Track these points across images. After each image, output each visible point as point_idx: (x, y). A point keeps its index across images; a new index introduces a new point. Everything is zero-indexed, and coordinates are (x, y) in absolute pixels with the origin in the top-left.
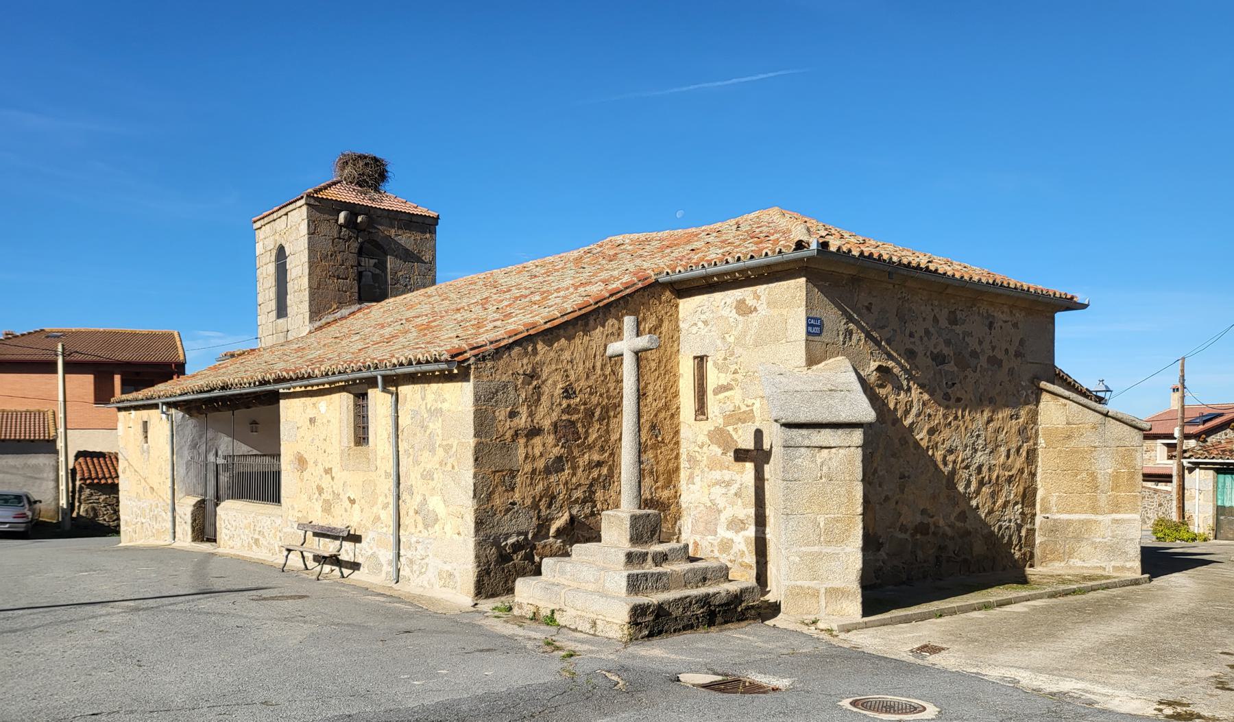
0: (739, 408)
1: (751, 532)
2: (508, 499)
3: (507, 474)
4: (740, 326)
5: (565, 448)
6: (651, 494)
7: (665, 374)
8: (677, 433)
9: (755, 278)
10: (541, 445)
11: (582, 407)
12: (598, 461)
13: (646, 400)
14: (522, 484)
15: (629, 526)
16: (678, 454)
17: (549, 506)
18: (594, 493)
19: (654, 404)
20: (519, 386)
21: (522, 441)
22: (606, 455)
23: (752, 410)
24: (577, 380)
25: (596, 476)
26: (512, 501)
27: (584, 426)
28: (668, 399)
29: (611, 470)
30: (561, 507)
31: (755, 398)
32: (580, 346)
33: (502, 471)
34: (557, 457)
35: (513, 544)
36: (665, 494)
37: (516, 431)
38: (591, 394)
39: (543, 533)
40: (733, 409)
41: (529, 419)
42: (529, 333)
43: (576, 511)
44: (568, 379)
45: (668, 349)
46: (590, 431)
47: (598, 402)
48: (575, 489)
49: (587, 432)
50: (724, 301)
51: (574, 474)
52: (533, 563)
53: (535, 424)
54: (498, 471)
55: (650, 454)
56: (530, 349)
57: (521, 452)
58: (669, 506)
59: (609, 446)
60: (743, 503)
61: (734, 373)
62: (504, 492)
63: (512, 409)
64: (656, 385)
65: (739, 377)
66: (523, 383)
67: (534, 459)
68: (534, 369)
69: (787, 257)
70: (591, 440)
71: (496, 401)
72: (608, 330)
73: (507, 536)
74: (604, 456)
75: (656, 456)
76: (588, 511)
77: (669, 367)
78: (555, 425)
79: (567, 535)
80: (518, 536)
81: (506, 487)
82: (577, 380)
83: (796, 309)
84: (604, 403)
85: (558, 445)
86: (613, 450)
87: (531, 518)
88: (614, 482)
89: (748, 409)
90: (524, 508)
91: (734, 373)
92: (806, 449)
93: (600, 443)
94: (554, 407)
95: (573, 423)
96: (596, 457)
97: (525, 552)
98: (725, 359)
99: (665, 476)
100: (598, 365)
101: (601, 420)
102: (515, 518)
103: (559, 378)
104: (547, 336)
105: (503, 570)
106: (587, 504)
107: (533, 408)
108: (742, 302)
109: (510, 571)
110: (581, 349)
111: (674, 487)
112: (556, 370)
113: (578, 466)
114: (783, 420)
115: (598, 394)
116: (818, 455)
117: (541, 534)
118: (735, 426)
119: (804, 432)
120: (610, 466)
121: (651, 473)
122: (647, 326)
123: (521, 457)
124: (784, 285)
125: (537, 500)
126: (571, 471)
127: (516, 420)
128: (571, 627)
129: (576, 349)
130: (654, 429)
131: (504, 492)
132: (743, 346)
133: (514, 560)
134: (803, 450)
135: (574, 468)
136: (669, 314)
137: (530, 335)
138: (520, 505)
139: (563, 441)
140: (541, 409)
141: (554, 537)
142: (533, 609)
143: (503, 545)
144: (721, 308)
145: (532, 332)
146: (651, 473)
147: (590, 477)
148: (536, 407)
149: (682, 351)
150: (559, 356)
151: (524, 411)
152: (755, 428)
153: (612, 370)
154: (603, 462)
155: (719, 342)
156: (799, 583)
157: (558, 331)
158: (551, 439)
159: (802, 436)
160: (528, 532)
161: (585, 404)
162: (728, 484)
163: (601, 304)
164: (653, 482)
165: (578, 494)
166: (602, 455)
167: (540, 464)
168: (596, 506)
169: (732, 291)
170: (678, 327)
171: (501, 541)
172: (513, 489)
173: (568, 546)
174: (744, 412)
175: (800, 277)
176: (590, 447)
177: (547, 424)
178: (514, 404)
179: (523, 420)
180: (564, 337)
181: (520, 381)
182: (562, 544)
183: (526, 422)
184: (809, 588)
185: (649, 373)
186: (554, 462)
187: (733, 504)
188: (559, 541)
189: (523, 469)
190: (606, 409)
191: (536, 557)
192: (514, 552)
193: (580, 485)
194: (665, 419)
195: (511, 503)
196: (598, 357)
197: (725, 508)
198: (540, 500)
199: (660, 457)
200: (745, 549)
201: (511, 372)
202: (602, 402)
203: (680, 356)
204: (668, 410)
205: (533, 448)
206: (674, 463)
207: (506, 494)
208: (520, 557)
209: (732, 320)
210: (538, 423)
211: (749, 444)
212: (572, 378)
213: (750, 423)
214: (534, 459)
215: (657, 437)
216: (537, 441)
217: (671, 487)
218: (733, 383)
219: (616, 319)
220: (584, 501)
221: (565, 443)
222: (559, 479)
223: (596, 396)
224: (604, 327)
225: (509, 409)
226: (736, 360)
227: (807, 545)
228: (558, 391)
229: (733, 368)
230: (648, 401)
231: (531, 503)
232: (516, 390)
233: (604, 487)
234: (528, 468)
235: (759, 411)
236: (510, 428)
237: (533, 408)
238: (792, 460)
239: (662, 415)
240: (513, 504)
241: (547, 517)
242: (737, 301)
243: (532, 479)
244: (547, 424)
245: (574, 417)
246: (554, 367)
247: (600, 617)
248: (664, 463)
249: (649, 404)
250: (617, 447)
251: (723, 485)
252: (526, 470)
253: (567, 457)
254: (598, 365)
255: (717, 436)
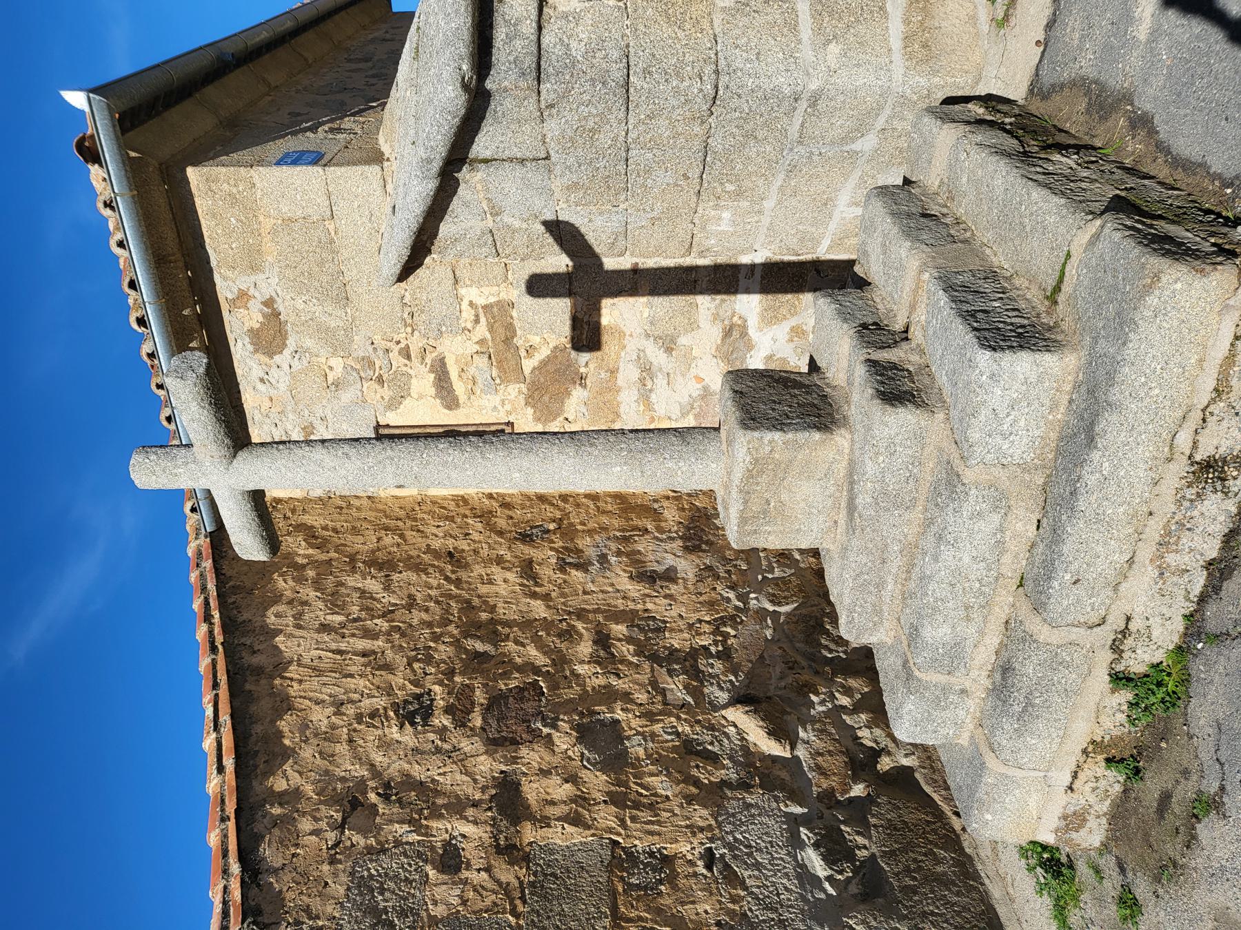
0: (482, 342)
1: (749, 305)
2: (695, 875)
3: (622, 878)
4: (308, 343)
5: (557, 719)
6: (673, 539)
7: (415, 520)
8: (542, 498)
9: (201, 301)
10: (545, 782)
11: (458, 679)
12: (595, 642)
13: (463, 551)
14: (652, 833)
15: (777, 436)
16: (587, 496)
17: (713, 759)
18: (673, 651)
19: (476, 536)
20: (372, 841)
21: (529, 834)
22: (580, 626)
23: (485, 307)
24: (389, 691)
25: (631, 648)
26: (700, 863)
27: (506, 675)
28: (468, 513)
29: (618, 616)
30: (712, 728)
31: (459, 299)
32: (306, 686)
33: (614, 894)
34: (577, 738)
35: (829, 860)
36: (671, 515)
37: (499, 850)
38: (429, 660)
39: (784, 775)
40: (486, 359)
41: (470, 812)
42: (232, 816)
43: (718, 693)
44: (382, 711)
45: (363, 515)
46: (518, 660)
47: (451, 644)
48: (665, 696)
49: (519, 669)
50: (260, 386)
51: (626, 697)
52: (869, 800)
53: (486, 797)
54: (614, 908)
55: (584, 542)
56: (276, 811)
57: (562, 836)
58: (698, 509)
59: (561, 621)
60: (686, 331)
61: (409, 357)
62: (675, 887)
63: (433, 863)
64: (433, 534)
65: (416, 343)
66: (364, 832)
67: (582, 800)
68: (334, 800)
69: (120, 182)
70: (541, 660)
71: (403, 914)
72: (287, 626)
73: (805, 877)
74: (583, 631)
75: (590, 532)
76: (718, 666)
77: (402, 513)
78: (494, 744)
79: (784, 712)
80: (801, 845)
81: (661, 882)
82: (389, 691)
83: (259, 194)
84: (455, 632)
85: (549, 735)
86: (569, 613)
87: (748, 806)
88: (646, 610)
89: (483, 319)
90: (719, 825)
91: (409, 357)
92: (544, 31)
93: (553, 641)
94: (446, 746)
95: (496, 702)
96: (585, 648)
97: (845, 823)
98: (380, 380)
99: (633, 516)
100: (362, 644)
101: (494, 637)
102: (750, 855)
103: (372, 735)
104: (256, 767)
105: (910, 891)
106: (702, 668)
107: (440, 801)
108: (255, 335)
109: (907, 870)
110: (315, 683)
111: (655, 501)
112: (350, 741)
113: (604, 687)
114: (465, 67)
115: (432, 644)
116: (561, 8)
117: (788, 778)
118: (523, 353)
119: (500, 34)
120: (606, 618)
121: (626, 539)
122: (301, 552)
123: (573, 836)
124: (209, 227)
125: (694, 790)
126: (618, 706)
127: (470, 851)
128: (1197, 589)
129: (312, 694)
130: (528, 536)
131: (675, 887)
132: (349, 330)
133: (873, 855)
134: (547, 40)
135: (609, 696)
136: (289, 514)
137: (238, 812)
138: (711, 840)
139: (539, 725)
140: (445, 782)
141: (793, 748)
142: (1097, 767)
143: (831, 891)
144: (273, 392)
145: (231, 808)
146: (626, 539)
147: (635, 660)
148: (438, 793)
149: (371, 491)
150: (316, 735)
151: (442, 828)
152: (528, 300)
153: (383, 616)
154: (598, 633)
155: (347, 396)
156: (896, 43)
157: (253, 739)
158: (531, 756)
159: (509, 39)
160: (787, 815)
161: (450, 673)
162: (647, 370)
163: (219, 639)
164: (646, 537)
165: (676, 688)
166: (581, 636)
167: (597, 781)
168: (705, 648)
169: (236, 365)
170: (320, 499)
171: (823, 896)
172: (667, 860)
173: (813, 712)
174: (491, 329)
175: (186, 181)
176: (561, 661)
177: (487, 765)
178: (419, 855)
179: (468, 829)
180: (273, 722)
181: (358, 839)
182: (809, 727)
183: (475, 823)
184: (907, 22)
185: (406, 548)
186: (591, 747)
187: (688, 360)
188: (802, 734)
189: (610, 830)
190: (472, 628)
191: (852, 794)
192: (849, 855)
193: (654, 683)
194: (512, 518)
195: (709, 867)
196: (343, 646)
197: (699, 379)
198: (696, 783)
199: (592, 525)
200: (786, 326)
201: (326, 868)
202: (452, 636)
203: (382, 494)
204: (491, 512)
205: (552, 803)
206: (606, 503)
207: (682, 882)
208: (860, 840)
209: (295, 363)
210: (484, 789)
211: (559, 310)
212: (380, 702)
213: (514, 314)
214: (582, 800)
215: (548, 531)
216: (532, 791)
217: (656, 506)
218: (428, 361)
219: (266, 609)
220: (695, 674)
221: (543, 719)
222: (638, 733)
223: (436, 650)
224: (278, 632)
225: (432, 873)
226: (380, 353)
227: (794, 28)
228: (408, 737)
229: (398, 361)
230: (467, 548)
231: (705, 806)
232: (384, 851)
233: (658, 630)
234: (606, 817)
235: (486, 290)
236: (488, 870)
237: (440, 801)
238: (574, 63)
239: (502, 523)
240: (709, 858)
241: (740, 764)
242: (256, 351)
243: (637, 806)
244: (487, 765)
245: (480, 696)
246: (342, 748)
247: (1184, 440)
248: (605, 520)
249: (473, 546)
250: (564, 604)
251: (649, 384)
252: (613, 823)
253: (581, 714)
254: (362, 644)
255: (546, 398)
